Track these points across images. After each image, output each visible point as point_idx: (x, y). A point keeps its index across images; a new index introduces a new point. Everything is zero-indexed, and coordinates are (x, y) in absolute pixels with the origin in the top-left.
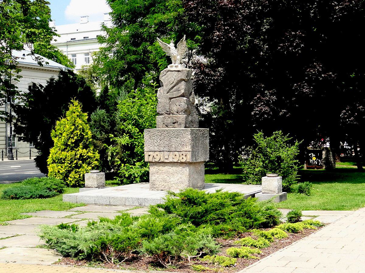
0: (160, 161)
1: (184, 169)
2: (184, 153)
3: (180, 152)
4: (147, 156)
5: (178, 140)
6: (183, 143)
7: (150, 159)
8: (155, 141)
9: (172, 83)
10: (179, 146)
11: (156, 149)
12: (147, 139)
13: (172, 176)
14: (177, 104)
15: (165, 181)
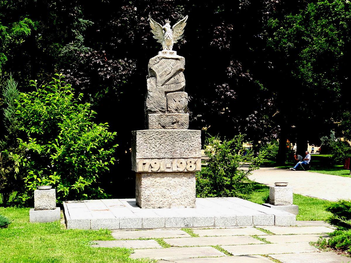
0: (159, 171)
1: (190, 180)
2: (193, 161)
3: (187, 158)
4: (140, 165)
5: (184, 143)
6: (191, 148)
7: (147, 169)
11: (154, 155)
13: (173, 189)
15: (164, 196)
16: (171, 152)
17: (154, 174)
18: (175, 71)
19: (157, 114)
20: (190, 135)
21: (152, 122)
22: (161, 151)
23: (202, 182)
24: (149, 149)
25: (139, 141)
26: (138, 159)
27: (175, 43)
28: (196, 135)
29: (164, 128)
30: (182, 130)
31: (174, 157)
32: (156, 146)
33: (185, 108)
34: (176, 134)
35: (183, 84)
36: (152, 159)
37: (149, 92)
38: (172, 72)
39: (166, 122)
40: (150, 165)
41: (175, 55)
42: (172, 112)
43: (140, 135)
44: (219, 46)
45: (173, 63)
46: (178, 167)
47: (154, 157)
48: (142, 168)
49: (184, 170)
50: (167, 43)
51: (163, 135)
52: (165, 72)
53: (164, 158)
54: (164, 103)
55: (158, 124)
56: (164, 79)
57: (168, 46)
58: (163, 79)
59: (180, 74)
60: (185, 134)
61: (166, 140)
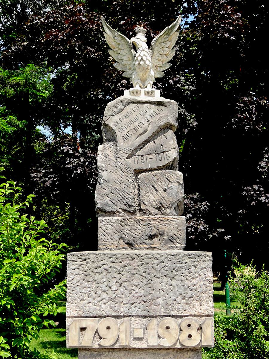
0: (116, 346)
2: (195, 322)
3: (181, 317)
5: (174, 282)
6: (190, 293)
8: (103, 286)
9: (142, 132)
10: (178, 300)
11: (106, 309)
12: (75, 281)
14: (160, 186)
16: (145, 302)
17: (107, 353)
18: (156, 128)
19: (117, 218)
20: (186, 263)
21: (104, 233)
22: (121, 300)
23: (224, 346)
24: (94, 295)
25: (72, 277)
26: (69, 317)
27: (159, 76)
28: (201, 262)
29: (130, 247)
30: (168, 252)
31: (151, 314)
32: (110, 288)
33: (178, 206)
34: (156, 262)
35: (174, 154)
36: (100, 317)
37: (101, 172)
38: (149, 128)
39: (136, 233)
40: (97, 331)
41: (157, 96)
42: (150, 214)
43: (74, 263)
44: (245, 125)
45: (152, 111)
46: (159, 337)
47: (106, 312)
48: (77, 338)
49: (175, 344)
50: (141, 74)
51: (126, 262)
52: (135, 129)
53: (129, 316)
54: (131, 196)
55: (117, 239)
56: (132, 145)
57: (144, 81)
58: (130, 143)
59: (166, 134)
61: (134, 274)
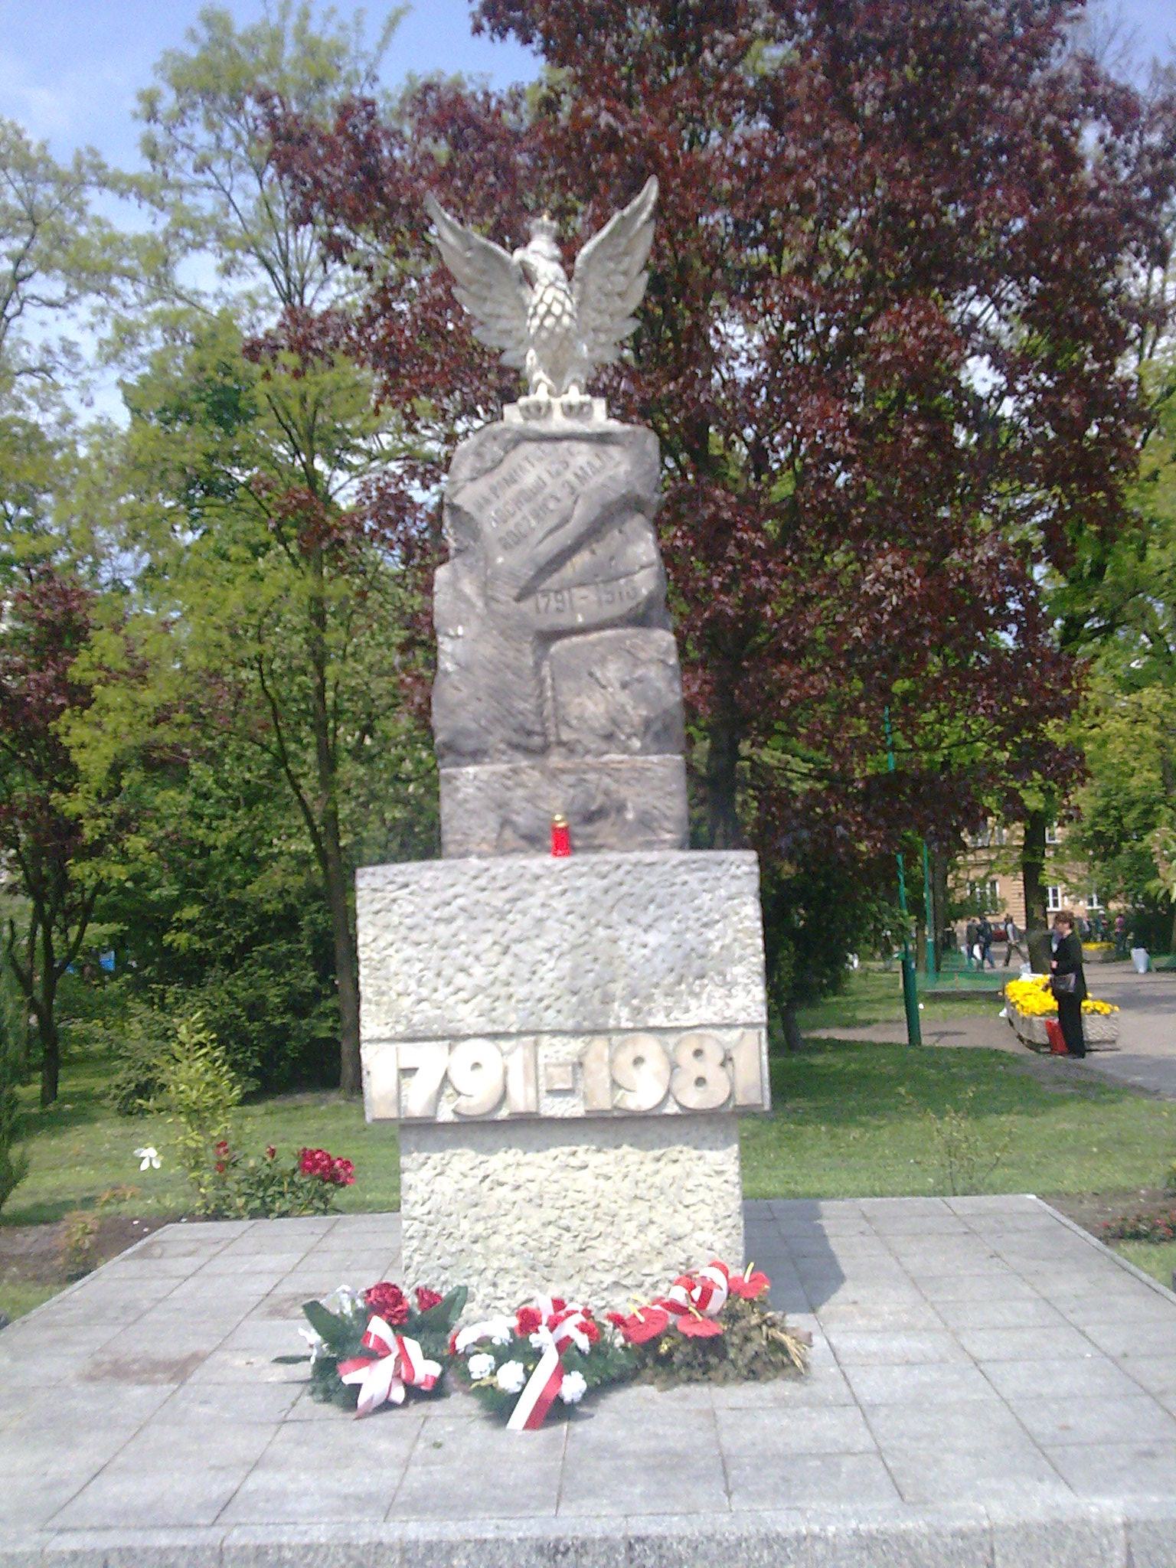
18: (597, 511)
35: (646, 582)
38: (578, 512)
41: (599, 415)
60: (653, 880)
